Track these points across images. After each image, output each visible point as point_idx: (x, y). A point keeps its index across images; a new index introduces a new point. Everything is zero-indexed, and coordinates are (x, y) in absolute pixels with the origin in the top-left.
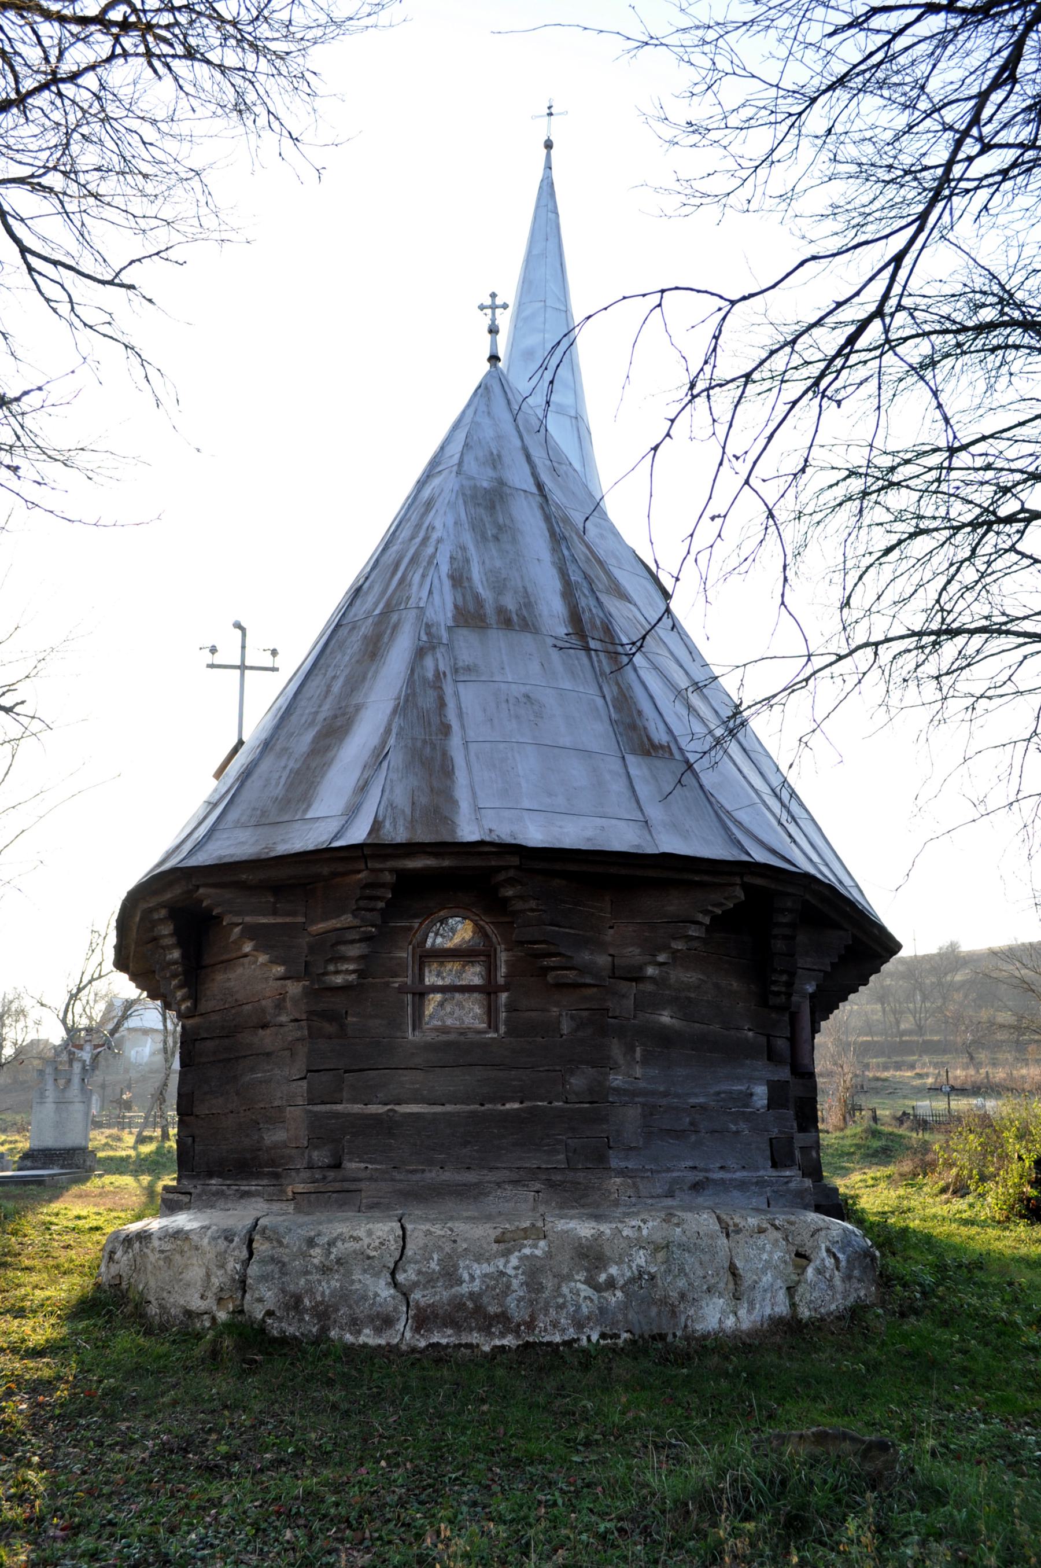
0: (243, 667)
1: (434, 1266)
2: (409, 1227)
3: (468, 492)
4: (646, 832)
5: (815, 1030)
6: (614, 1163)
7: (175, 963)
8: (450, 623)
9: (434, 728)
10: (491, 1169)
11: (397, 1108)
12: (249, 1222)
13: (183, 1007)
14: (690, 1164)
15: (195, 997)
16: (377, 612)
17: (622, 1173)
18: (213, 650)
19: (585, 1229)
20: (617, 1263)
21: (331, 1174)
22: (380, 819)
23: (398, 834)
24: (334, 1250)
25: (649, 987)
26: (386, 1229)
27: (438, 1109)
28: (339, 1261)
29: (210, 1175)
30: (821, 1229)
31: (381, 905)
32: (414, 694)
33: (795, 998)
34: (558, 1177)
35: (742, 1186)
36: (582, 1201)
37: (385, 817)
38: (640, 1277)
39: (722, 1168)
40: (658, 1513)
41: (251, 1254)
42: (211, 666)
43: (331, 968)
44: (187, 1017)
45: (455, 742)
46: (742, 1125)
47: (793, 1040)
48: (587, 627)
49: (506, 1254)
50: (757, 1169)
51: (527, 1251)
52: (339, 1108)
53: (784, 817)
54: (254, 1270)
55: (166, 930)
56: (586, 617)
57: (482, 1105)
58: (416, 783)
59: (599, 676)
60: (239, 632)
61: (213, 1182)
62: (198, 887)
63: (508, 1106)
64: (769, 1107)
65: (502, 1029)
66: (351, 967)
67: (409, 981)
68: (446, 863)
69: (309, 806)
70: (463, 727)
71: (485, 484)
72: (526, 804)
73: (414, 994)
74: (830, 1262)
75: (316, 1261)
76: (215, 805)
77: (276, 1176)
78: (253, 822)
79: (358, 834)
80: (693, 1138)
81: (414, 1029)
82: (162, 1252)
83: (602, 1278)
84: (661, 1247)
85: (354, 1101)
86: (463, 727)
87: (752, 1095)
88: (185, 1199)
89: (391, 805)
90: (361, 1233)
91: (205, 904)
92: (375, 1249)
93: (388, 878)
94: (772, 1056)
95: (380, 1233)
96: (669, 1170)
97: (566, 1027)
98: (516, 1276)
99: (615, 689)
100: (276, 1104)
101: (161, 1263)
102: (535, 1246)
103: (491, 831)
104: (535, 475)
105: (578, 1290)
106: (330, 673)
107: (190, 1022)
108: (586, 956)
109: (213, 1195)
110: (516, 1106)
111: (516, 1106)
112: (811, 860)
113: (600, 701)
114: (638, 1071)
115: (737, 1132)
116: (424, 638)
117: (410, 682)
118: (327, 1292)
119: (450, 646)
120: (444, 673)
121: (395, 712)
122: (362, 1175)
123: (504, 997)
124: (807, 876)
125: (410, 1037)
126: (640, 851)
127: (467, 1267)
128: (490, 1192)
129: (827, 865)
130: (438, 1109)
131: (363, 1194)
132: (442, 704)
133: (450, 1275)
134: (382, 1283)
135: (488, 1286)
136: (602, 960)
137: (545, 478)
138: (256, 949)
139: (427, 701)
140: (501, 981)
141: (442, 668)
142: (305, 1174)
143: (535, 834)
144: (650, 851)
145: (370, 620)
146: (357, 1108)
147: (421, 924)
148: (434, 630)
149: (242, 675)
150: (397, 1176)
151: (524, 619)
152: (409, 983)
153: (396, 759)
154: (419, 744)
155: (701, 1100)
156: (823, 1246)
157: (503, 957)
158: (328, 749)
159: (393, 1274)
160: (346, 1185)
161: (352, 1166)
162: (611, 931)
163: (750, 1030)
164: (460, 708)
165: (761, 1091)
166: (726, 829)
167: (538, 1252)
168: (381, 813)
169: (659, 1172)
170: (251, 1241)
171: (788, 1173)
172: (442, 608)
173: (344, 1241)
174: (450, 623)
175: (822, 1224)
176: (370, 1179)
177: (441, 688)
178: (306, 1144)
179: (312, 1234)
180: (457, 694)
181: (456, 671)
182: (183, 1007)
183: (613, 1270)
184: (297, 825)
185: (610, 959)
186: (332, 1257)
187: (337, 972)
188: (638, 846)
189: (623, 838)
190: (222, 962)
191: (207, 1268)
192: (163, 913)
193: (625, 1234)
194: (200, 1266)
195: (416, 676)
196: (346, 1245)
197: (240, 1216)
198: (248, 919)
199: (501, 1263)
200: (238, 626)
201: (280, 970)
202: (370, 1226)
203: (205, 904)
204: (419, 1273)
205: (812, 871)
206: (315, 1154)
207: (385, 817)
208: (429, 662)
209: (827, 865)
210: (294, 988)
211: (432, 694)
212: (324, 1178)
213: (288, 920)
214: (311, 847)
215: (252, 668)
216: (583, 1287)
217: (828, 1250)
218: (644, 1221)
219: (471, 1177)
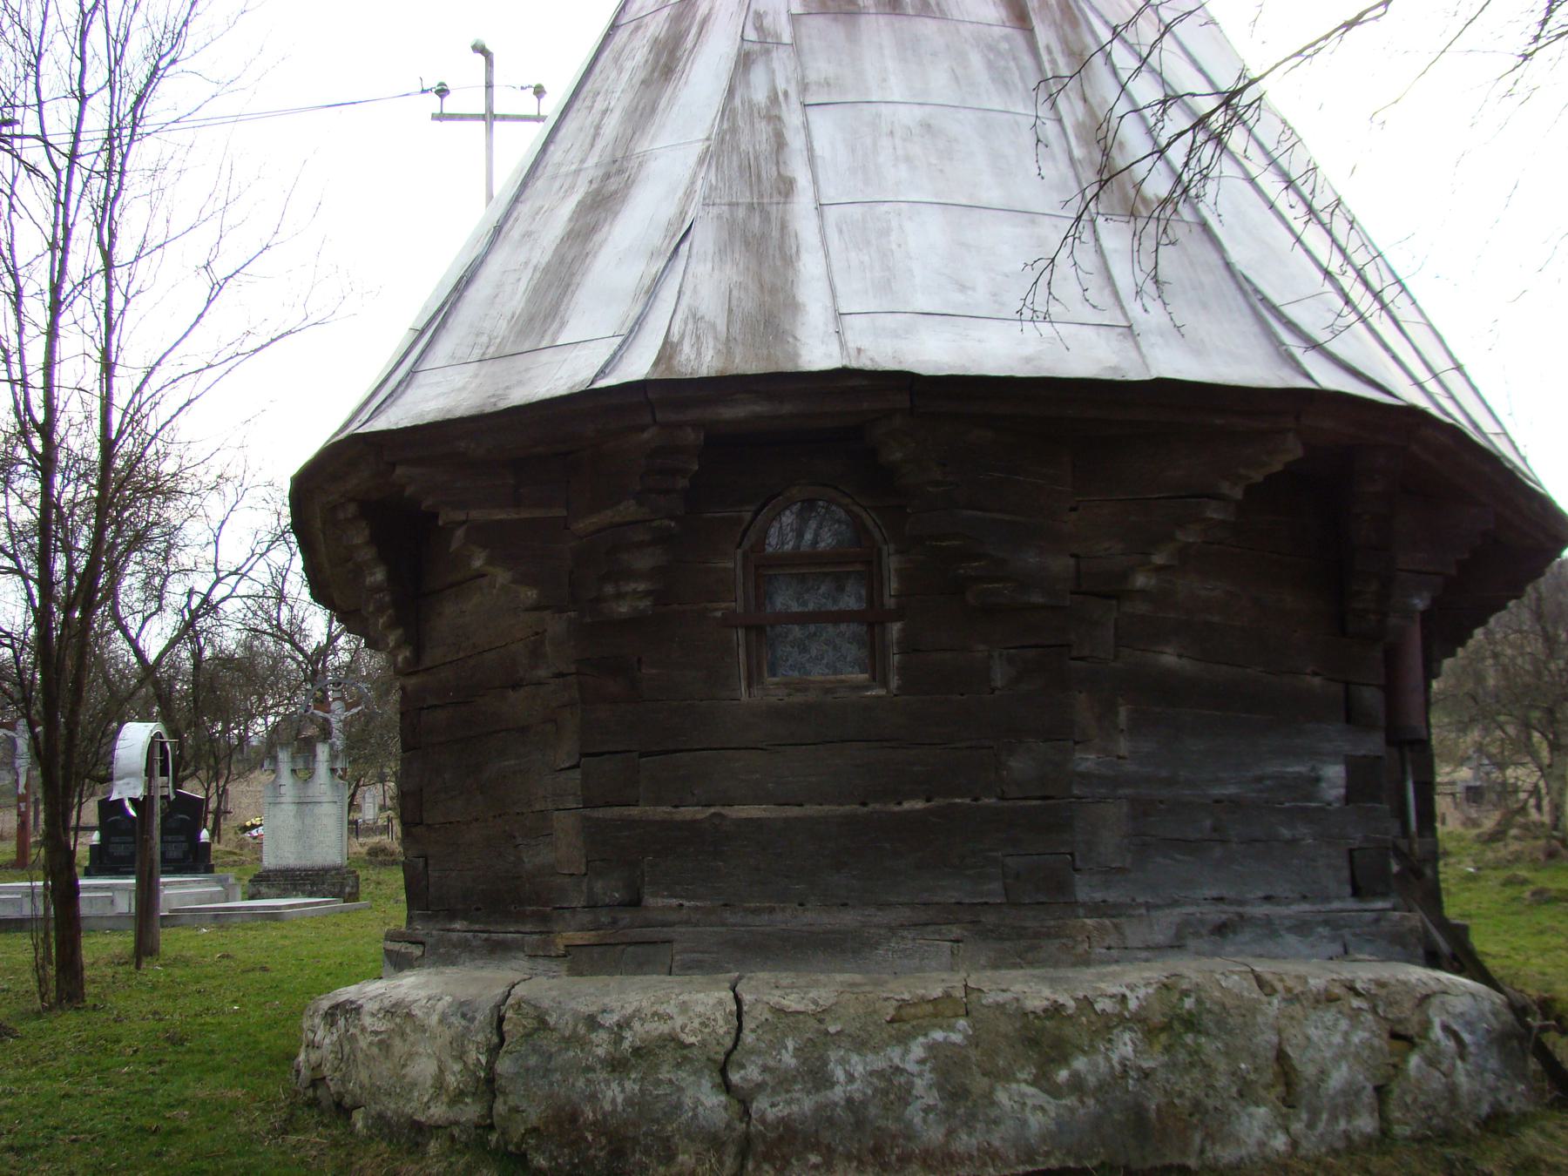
0: (489, 117)
1: (788, 1059)
2: (747, 998)
4: (1129, 344)
5: (1431, 672)
6: (1082, 894)
7: (378, 589)
9: (766, 185)
10: (881, 906)
11: (726, 811)
12: (499, 991)
13: (400, 658)
14: (1215, 893)
15: (416, 640)
17: (1098, 909)
18: (442, 92)
19: (1031, 990)
20: (1085, 1053)
21: (626, 917)
22: (675, 339)
23: (702, 361)
24: (628, 1034)
25: (1141, 608)
26: (711, 1002)
27: (795, 811)
28: (637, 1051)
29: (452, 915)
30: (1434, 993)
31: (682, 483)
32: (734, 130)
33: (1393, 621)
34: (989, 919)
35: (1302, 928)
36: (1030, 956)
37: (682, 337)
38: (1125, 1072)
39: (1268, 899)
41: (502, 1041)
42: (440, 117)
43: (609, 589)
44: (409, 674)
45: (803, 202)
46: (1303, 830)
47: (1392, 690)
49: (903, 1040)
50: (1327, 899)
51: (938, 1035)
52: (634, 811)
53: (1349, 281)
54: (504, 1065)
55: (359, 536)
57: (864, 804)
58: (735, 278)
59: (1048, 89)
60: (481, 58)
61: (457, 926)
62: (393, 465)
63: (906, 805)
64: (1348, 799)
65: (894, 682)
66: (642, 587)
67: (739, 607)
68: (787, 408)
69: (563, 325)
70: (815, 181)
72: (923, 304)
73: (748, 628)
74: (1449, 1044)
75: (600, 1051)
76: (422, 332)
77: (544, 918)
79: (638, 367)
80: (1218, 852)
81: (749, 686)
82: (376, 1033)
83: (1063, 1075)
84: (1175, 1024)
85: (658, 802)
86: (815, 181)
87: (1318, 780)
88: (417, 951)
90: (671, 1009)
91: (408, 491)
92: (694, 1033)
93: (691, 437)
94: (1352, 716)
95: (700, 1009)
96: (1175, 903)
97: (1000, 676)
98: (921, 1075)
99: (1079, 106)
100: (537, 807)
101: (375, 1050)
102: (952, 1028)
103: (859, 350)
105: (1023, 1095)
106: (600, 105)
107: (412, 682)
108: (1032, 559)
109: (455, 946)
110: (919, 805)
111: (919, 805)
112: (1420, 385)
114: (1123, 746)
115: (1293, 841)
116: (751, 35)
117: (727, 111)
118: (620, 1099)
119: (796, 47)
120: (786, 94)
121: (701, 161)
122: (673, 917)
123: (895, 629)
124: (1412, 412)
125: (744, 697)
126: (1118, 377)
127: (843, 1061)
128: (878, 943)
129: (1452, 397)
130: (795, 811)
131: (677, 947)
132: (780, 143)
133: (818, 1077)
134: (706, 1084)
135: (876, 1090)
136: (1061, 565)
138: (490, 561)
139: (756, 138)
140: (890, 603)
141: (781, 85)
142: (586, 918)
143: (935, 352)
144: (1147, 378)
145: (666, 11)
146: (661, 812)
147: (756, 513)
148: (767, 22)
149: (489, 130)
150: (731, 918)
152: (740, 610)
153: (705, 238)
154: (741, 213)
155: (1232, 790)
156: (1437, 1022)
157: (892, 563)
158: (593, 229)
160: (649, 933)
161: (656, 902)
162: (1074, 515)
163: (1315, 674)
164: (810, 149)
165: (1334, 774)
166: (1278, 344)
167: (956, 1038)
168: (676, 330)
169: (1157, 907)
170: (501, 1020)
171: (1380, 905)
173: (643, 1020)
175: (1434, 986)
176: (687, 923)
177: (779, 118)
178: (583, 869)
179: (594, 1009)
180: (806, 126)
181: (804, 87)
182: (400, 658)
183: (1080, 1063)
184: (545, 356)
185: (1072, 561)
186: (626, 1044)
187: (620, 596)
188: (1115, 369)
189: (1087, 354)
190: (451, 586)
191: (439, 1060)
192: (352, 509)
193: (1098, 1007)
194: (429, 1056)
195: (737, 102)
196: (647, 1026)
198: (475, 514)
199: (895, 1053)
200: (480, 49)
201: (530, 594)
202: (684, 997)
203: (408, 491)
204: (765, 1069)
205: (1421, 402)
206: (599, 886)
207: (682, 337)
208: (758, 76)
209: (1452, 397)
210: (556, 625)
211: (764, 129)
212: (614, 922)
213: (538, 513)
214: (561, 390)
215: (504, 118)
216: (1030, 1090)
217: (1446, 1028)
218: (1132, 987)
219: (848, 919)
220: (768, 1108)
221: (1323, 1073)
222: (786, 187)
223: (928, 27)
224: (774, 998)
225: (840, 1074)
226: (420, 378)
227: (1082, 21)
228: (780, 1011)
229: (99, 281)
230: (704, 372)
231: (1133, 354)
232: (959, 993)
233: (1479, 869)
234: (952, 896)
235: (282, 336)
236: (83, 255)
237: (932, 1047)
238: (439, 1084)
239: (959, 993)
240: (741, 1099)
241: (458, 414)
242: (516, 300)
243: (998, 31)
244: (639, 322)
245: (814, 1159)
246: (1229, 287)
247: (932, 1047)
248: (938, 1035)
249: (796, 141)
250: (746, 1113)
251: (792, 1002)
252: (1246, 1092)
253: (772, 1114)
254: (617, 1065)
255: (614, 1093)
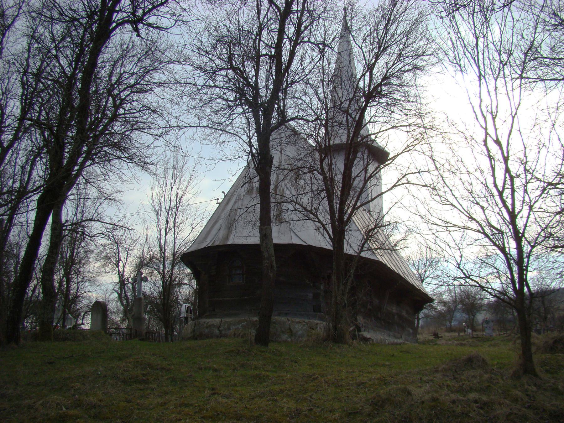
1: (226, 327)
49: (239, 324)
221: (297, 331)
229: (173, 230)
231: (558, 190)
234: (297, 320)
235: (480, 93)
236: (171, 224)
251: (227, 320)
252: (283, 332)
254: (207, 328)
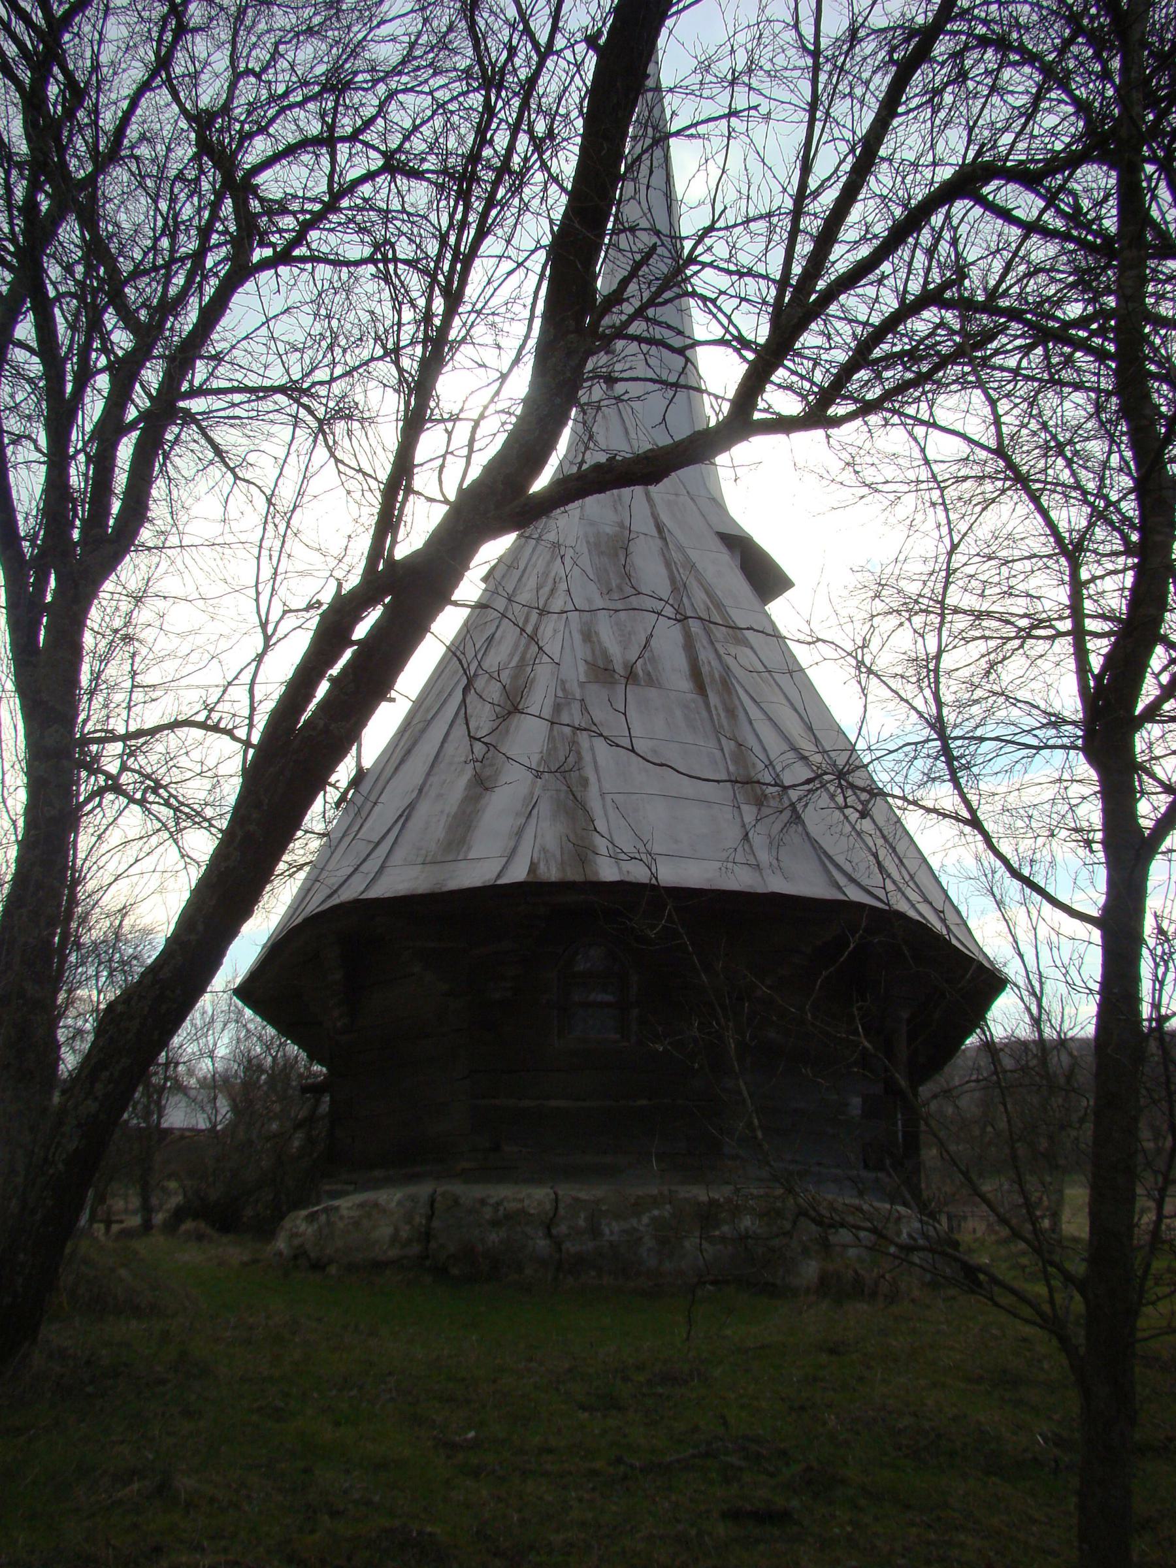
1: (581, 1223)
3: (592, 540)
8: (582, 679)
16: (513, 664)
19: (700, 1193)
23: (551, 873)
39: (819, 1164)
40: (672, 498)
45: (593, 790)
48: (707, 680)
51: (656, 1212)
54: (436, 1224)
56: (705, 670)
69: (469, 849)
71: (608, 530)
78: (420, 860)
79: (518, 873)
88: (351, 1188)
89: (544, 850)
104: (655, 517)
113: (718, 753)
116: (560, 694)
133: (594, 1231)
137: (664, 518)
144: (760, 891)
148: (568, 686)
151: (649, 674)
153: (545, 808)
159: (548, 1228)
164: (595, 762)
165: (856, 1103)
172: (575, 671)
174: (582, 679)
180: (592, 748)
183: (726, 1229)
184: (463, 864)
189: (741, 880)
197: (424, 1190)
220: (571, 1247)
222: (585, 782)
223: (653, 693)
224: (574, 1193)
225: (607, 1231)
226: (388, 871)
227: (741, 715)
228: (577, 1200)
230: (553, 879)
232: (666, 1192)
233: (992, 1260)
237: (654, 1219)
238: (394, 1239)
239: (666, 1192)
240: (558, 1244)
241: (420, 891)
242: (439, 831)
243: (690, 696)
244: (514, 851)
245: (593, 1273)
246: (807, 845)
247: (654, 1219)
248: (656, 1212)
249: (587, 757)
250: (560, 1250)
251: (583, 1195)
253: (573, 1250)
254: (495, 1223)
255: (494, 1237)
